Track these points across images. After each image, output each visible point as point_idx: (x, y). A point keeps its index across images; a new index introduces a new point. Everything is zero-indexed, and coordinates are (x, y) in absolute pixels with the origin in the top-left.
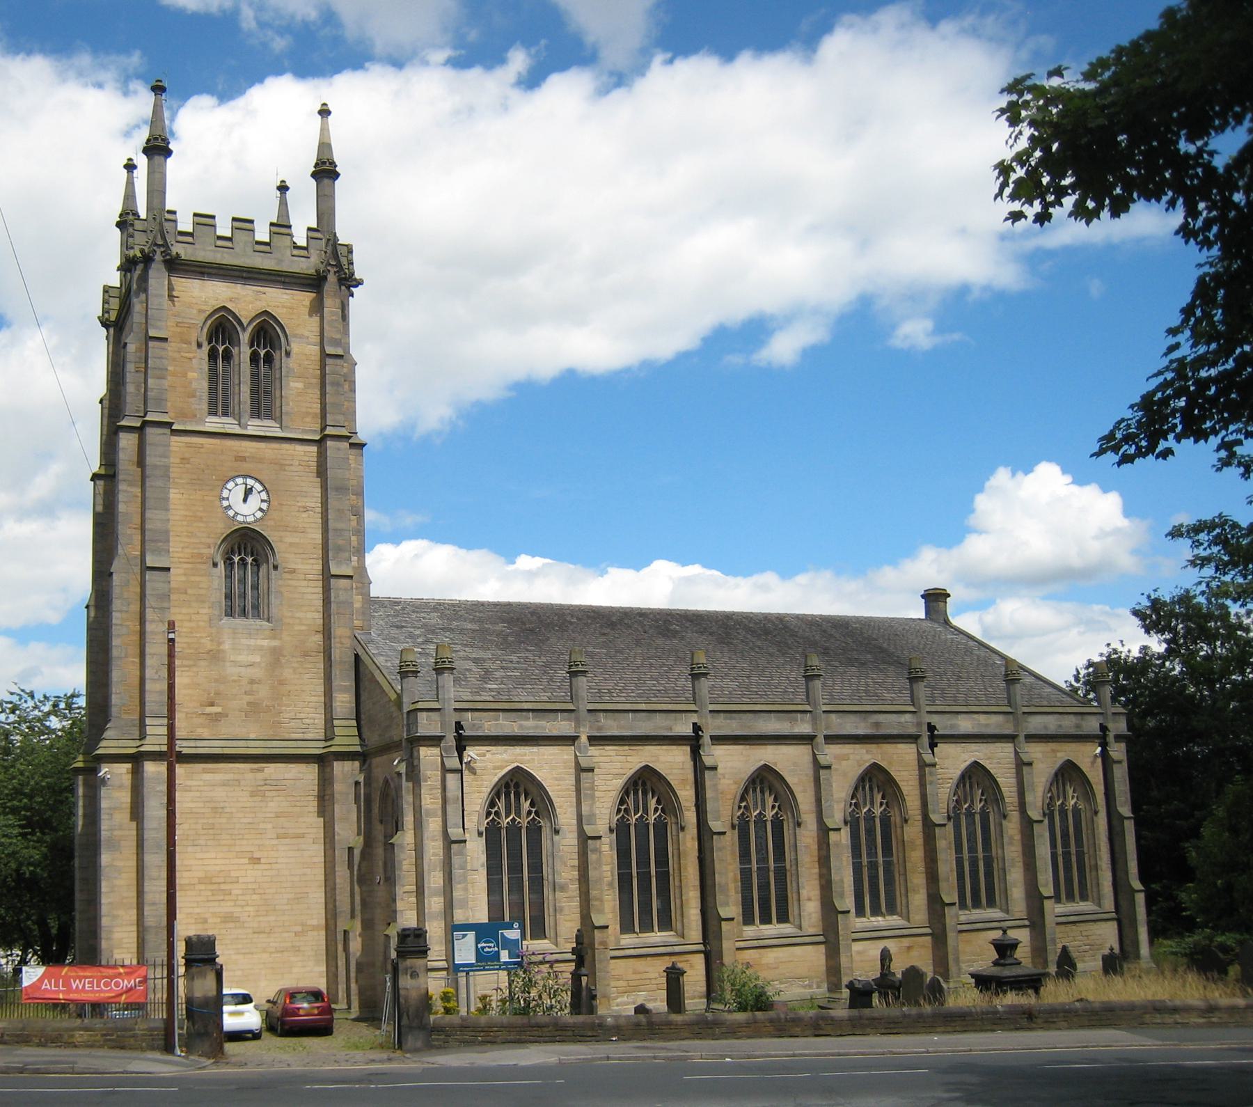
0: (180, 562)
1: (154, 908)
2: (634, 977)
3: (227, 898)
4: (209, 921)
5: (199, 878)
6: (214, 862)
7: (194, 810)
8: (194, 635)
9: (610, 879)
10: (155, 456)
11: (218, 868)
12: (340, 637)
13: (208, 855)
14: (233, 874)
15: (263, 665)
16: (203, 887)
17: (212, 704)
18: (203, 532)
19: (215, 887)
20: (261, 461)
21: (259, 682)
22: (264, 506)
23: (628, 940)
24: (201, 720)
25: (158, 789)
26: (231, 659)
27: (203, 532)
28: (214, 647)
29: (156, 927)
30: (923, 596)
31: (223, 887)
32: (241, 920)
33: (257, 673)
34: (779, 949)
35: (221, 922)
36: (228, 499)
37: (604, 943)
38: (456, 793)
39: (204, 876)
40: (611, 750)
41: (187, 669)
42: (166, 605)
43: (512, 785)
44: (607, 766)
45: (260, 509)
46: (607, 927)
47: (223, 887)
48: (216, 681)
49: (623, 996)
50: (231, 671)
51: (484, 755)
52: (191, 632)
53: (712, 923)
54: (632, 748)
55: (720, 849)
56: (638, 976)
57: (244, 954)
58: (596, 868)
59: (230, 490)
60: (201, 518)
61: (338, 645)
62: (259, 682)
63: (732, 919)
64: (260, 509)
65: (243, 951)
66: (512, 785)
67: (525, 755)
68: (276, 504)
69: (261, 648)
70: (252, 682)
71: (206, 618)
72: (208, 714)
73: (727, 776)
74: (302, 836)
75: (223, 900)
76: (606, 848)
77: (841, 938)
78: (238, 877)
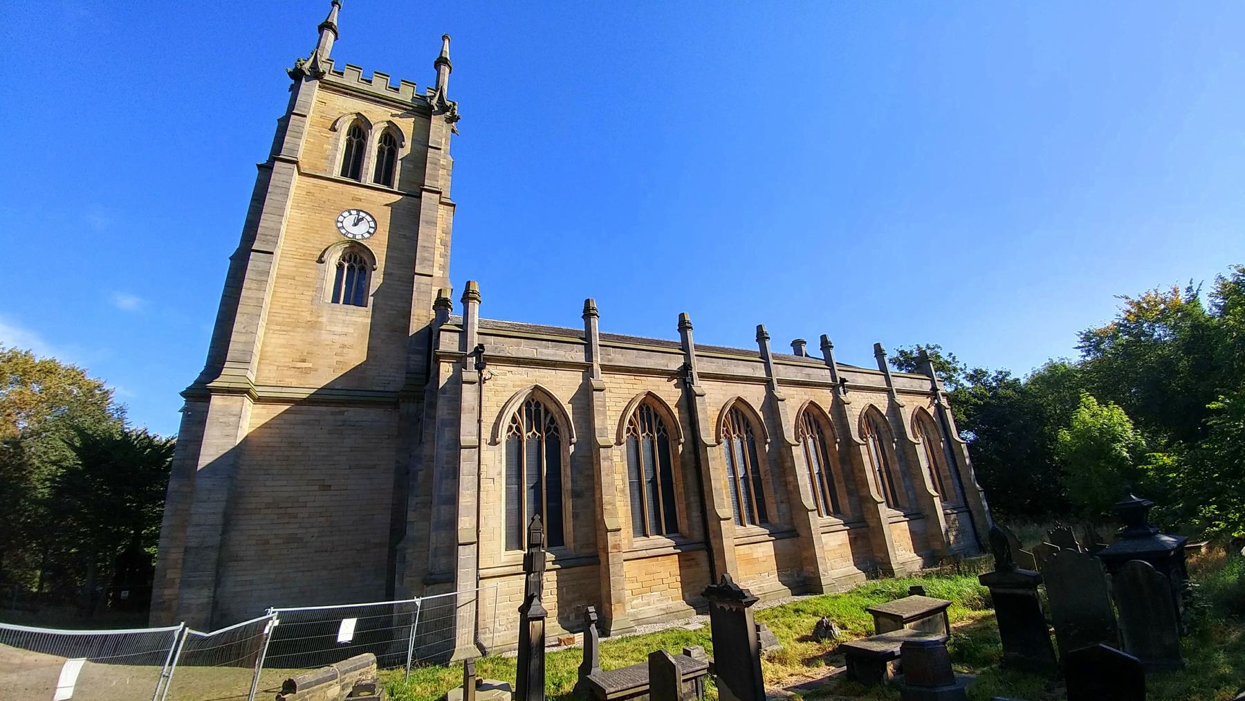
0: (293, 258)
1: (198, 529)
2: (647, 578)
3: (292, 520)
4: (271, 542)
5: (266, 504)
6: (284, 489)
7: (270, 444)
8: (296, 309)
9: (622, 486)
10: (279, 181)
11: (287, 495)
12: (418, 316)
13: (279, 483)
14: (301, 499)
15: (356, 335)
16: (269, 511)
17: (304, 361)
18: (318, 240)
19: (282, 511)
20: (373, 203)
21: (351, 347)
22: (372, 231)
23: (640, 542)
24: (292, 372)
25: (221, 421)
26: (328, 329)
27: (318, 240)
28: (313, 319)
29: (197, 548)
30: (791, 345)
31: (289, 511)
32: (305, 540)
33: (348, 341)
34: (651, 555)
35: (284, 543)
36: (342, 222)
37: (617, 547)
38: (473, 403)
39: (271, 501)
40: (620, 378)
41: (284, 333)
42: (263, 278)
43: (533, 404)
44: (616, 390)
45: (368, 232)
46: (619, 530)
47: (289, 511)
48: (310, 343)
49: (637, 598)
50: (325, 337)
51: (505, 375)
52: (294, 307)
53: (712, 524)
54: (637, 378)
55: (714, 459)
56: (651, 577)
57: (303, 572)
58: (607, 475)
59: (345, 217)
60: (317, 231)
61: (416, 321)
62: (351, 347)
63: (729, 519)
64: (368, 232)
65: (303, 569)
66: (533, 404)
67: (544, 377)
68: (382, 230)
69: (355, 323)
70: (344, 346)
71: (310, 298)
72: (298, 368)
73: (711, 404)
74: (374, 467)
75: (288, 523)
76: (617, 459)
77: (813, 532)
78: (306, 502)
